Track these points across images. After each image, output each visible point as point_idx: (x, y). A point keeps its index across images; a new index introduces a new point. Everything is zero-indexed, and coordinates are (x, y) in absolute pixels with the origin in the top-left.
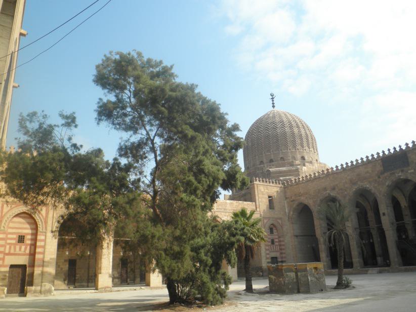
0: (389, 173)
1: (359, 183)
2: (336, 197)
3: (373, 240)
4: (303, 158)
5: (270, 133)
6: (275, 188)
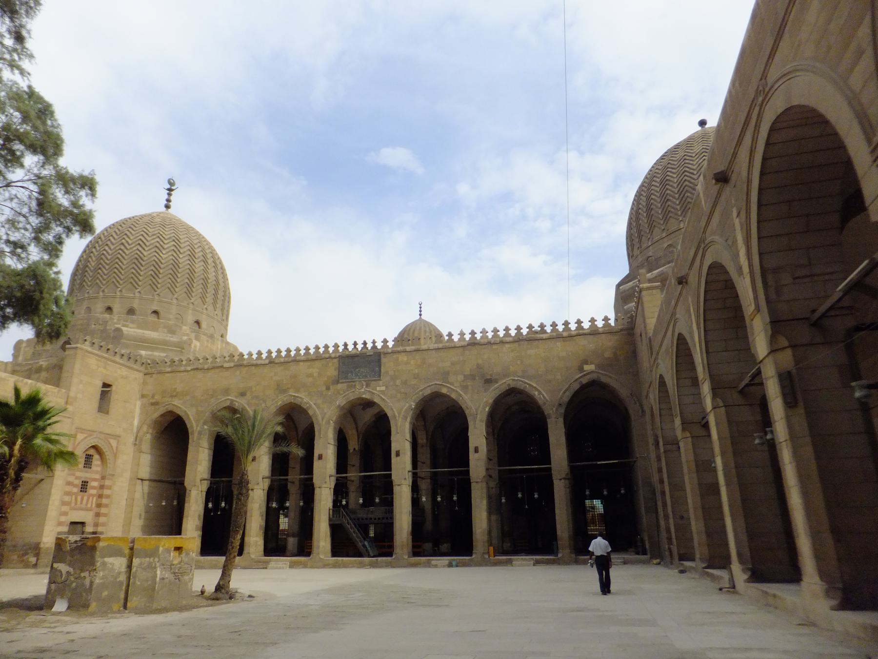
5: (145, 253)
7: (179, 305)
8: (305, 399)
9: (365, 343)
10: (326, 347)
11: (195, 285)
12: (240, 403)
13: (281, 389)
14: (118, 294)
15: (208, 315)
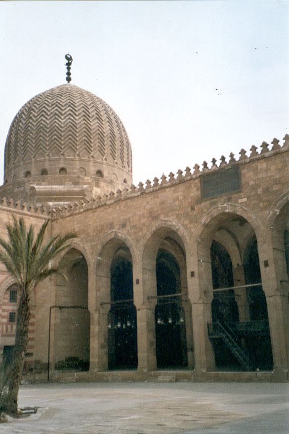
0: (208, 202)
1: (162, 217)
2: (125, 240)
3: (184, 319)
4: (100, 173)
5: (48, 122)
6: (32, 219)
7: (81, 160)
8: (174, 222)
9: (223, 158)
10: (188, 169)
11: (92, 141)
12: (122, 234)
13: (153, 216)
14: (33, 160)
15: (108, 165)
